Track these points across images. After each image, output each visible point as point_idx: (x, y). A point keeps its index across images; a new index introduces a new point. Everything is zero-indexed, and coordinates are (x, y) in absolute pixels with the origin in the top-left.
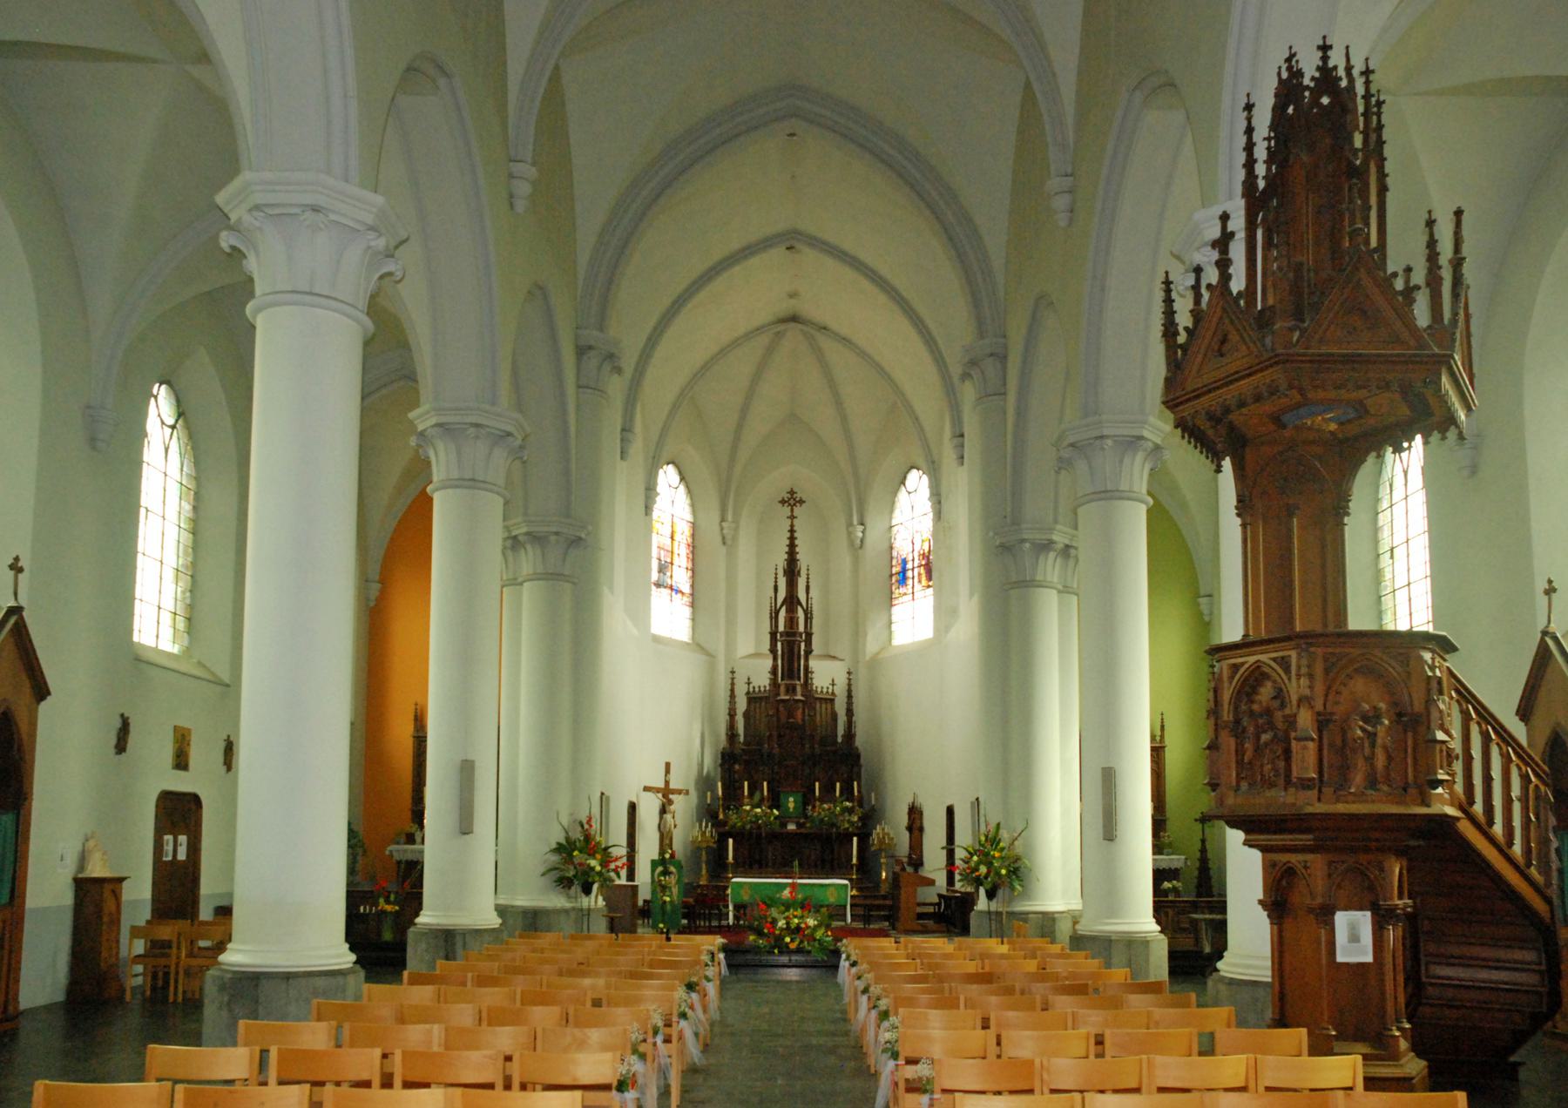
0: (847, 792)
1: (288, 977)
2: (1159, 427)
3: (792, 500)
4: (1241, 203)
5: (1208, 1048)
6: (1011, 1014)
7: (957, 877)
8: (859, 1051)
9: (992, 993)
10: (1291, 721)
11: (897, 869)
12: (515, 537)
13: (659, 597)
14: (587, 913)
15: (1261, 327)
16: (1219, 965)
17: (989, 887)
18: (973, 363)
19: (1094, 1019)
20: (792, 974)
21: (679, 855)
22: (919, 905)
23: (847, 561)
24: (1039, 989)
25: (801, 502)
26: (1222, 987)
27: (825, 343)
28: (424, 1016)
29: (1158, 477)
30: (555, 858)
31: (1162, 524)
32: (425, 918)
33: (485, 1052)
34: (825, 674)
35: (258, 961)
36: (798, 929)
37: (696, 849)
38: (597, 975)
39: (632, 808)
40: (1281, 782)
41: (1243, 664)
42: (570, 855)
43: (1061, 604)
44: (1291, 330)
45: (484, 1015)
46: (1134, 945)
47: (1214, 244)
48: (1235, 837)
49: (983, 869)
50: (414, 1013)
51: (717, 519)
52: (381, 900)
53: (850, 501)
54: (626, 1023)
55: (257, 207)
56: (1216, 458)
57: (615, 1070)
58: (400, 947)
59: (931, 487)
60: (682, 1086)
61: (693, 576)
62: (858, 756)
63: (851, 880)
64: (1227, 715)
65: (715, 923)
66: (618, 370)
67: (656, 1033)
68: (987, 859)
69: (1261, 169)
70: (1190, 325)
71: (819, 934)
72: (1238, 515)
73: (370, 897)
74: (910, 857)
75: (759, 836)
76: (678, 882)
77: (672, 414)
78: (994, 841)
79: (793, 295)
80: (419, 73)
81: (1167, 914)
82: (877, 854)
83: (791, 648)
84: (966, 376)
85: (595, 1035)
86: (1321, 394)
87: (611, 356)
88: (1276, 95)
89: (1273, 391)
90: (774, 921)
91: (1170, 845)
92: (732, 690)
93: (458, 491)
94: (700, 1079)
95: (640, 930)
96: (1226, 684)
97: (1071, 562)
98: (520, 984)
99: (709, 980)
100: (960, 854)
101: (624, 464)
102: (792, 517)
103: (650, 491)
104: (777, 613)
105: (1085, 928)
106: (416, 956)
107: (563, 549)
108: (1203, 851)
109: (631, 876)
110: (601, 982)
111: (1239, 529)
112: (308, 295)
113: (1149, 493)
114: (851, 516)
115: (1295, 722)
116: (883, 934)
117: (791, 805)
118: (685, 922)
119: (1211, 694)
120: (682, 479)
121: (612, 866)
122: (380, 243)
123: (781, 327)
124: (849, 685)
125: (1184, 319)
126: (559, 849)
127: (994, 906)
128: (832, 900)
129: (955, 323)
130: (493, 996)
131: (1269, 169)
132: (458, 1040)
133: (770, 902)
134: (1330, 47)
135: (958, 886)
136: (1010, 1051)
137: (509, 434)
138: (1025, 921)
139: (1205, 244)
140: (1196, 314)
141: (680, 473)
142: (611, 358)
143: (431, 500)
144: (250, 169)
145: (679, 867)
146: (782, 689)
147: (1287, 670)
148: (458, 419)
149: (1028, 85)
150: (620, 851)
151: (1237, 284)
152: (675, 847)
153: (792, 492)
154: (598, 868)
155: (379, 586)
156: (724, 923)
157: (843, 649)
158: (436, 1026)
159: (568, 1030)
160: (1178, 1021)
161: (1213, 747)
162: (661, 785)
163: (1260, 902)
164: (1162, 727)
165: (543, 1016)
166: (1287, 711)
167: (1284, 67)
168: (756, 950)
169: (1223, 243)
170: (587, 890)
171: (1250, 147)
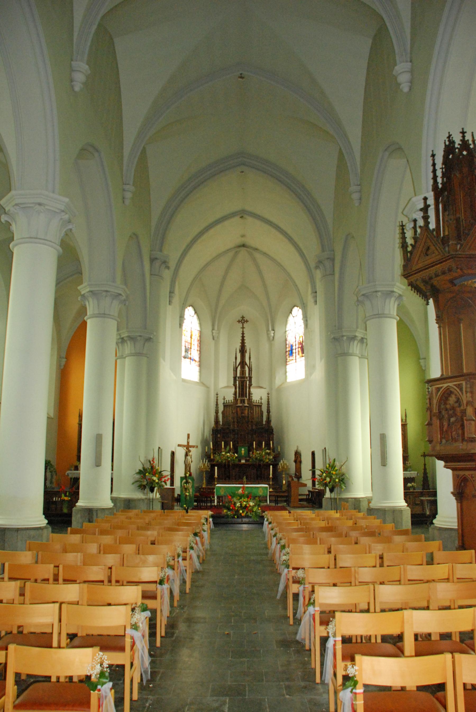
0: (268, 445)
1: (18, 530)
2: (401, 286)
3: (243, 321)
4: (432, 194)
5: (430, 561)
6: (341, 546)
7: (317, 483)
8: (272, 561)
9: (333, 537)
10: (464, 412)
11: (290, 479)
12: (123, 338)
13: (185, 363)
14: (151, 501)
15: (443, 244)
16: (434, 521)
17: (331, 487)
18: (320, 262)
19: (378, 548)
20: (245, 527)
21: (194, 475)
22: (300, 495)
23: (267, 346)
24: (354, 534)
25: (247, 321)
26: (436, 532)
27: (257, 255)
28: (75, 549)
29: (401, 308)
30: (138, 476)
31: (403, 327)
32: (81, 503)
33: (100, 567)
34: (257, 395)
35: (7, 523)
36: (246, 507)
37: (201, 472)
38: (154, 530)
39: (173, 454)
40: (460, 438)
41: (442, 387)
42: (145, 475)
43: (360, 363)
44: (456, 245)
45: (102, 548)
46: (395, 512)
47: (421, 210)
48: (440, 464)
49: (328, 479)
50: (72, 547)
51: (210, 328)
52: (63, 495)
53: (268, 320)
54: (166, 551)
55: (16, 205)
56: (426, 298)
57: (158, 575)
58: (70, 515)
59: (303, 314)
60: (192, 579)
61: (200, 354)
62: (272, 430)
63: (269, 484)
64: (435, 410)
65: (209, 504)
66: (168, 268)
67: (179, 556)
68: (330, 476)
69: (439, 180)
70: (413, 243)
71: (255, 509)
72: (437, 323)
73: (58, 494)
74: (296, 475)
75: (229, 465)
76: (192, 487)
77: (192, 285)
78: (332, 466)
79: (243, 236)
80: (87, 151)
81: (410, 498)
82: (281, 473)
83: (242, 383)
84: (317, 267)
85: (151, 558)
86: (470, 271)
87: (165, 262)
88: (444, 151)
89: (450, 270)
90: (235, 504)
91: (410, 467)
92: (217, 402)
93: (97, 319)
94: (200, 575)
95: (176, 508)
96: (434, 396)
97: (365, 344)
98: (120, 533)
99: (204, 531)
100: (318, 473)
101: (170, 307)
102: (243, 328)
103: (182, 317)
104: (237, 368)
105: (373, 505)
106: (76, 519)
107: (143, 342)
108: (425, 469)
109: (172, 484)
110: (155, 533)
111: (438, 329)
112: (33, 239)
113: (397, 315)
114: (268, 326)
115: (465, 413)
116: (283, 509)
117: (243, 452)
118: (196, 504)
119: (428, 401)
120: (196, 313)
121: (163, 480)
122: (66, 217)
123: (238, 250)
124: (268, 399)
125: (410, 241)
126: (140, 472)
127: (333, 495)
128: (261, 494)
129: (312, 247)
130: (107, 540)
131: (443, 180)
132: (89, 561)
133: (233, 495)
134: (466, 132)
135: (317, 487)
136: (340, 564)
137: (120, 295)
138: (347, 502)
139: (418, 211)
140: (415, 239)
141: (195, 310)
142: (165, 263)
143: (86, 323)
144: (15, 190)
145: (193, 480)
146: (239, 401)
147: (461, 390)
148: (98, 289)
149: (341, 153)
150: (167, 473)
151: (432, 226)
152: (192, 471)
153: (243, 317)
154: (157, 481)
155: (65, 360)
156: (213, 504)
157: (265, 383)
158: (79, 554)
159: (138, 556)
160: (416, 548)
161: (429, 424)
162: (186, 444)
163: (452, 493)
164: (406, 415)
165: (129, 549)
166: (462, 408)
167: (447, 140)
168: (227, 516)
169: (425, 209)
170: (152, 490)
171: (434, 171)
